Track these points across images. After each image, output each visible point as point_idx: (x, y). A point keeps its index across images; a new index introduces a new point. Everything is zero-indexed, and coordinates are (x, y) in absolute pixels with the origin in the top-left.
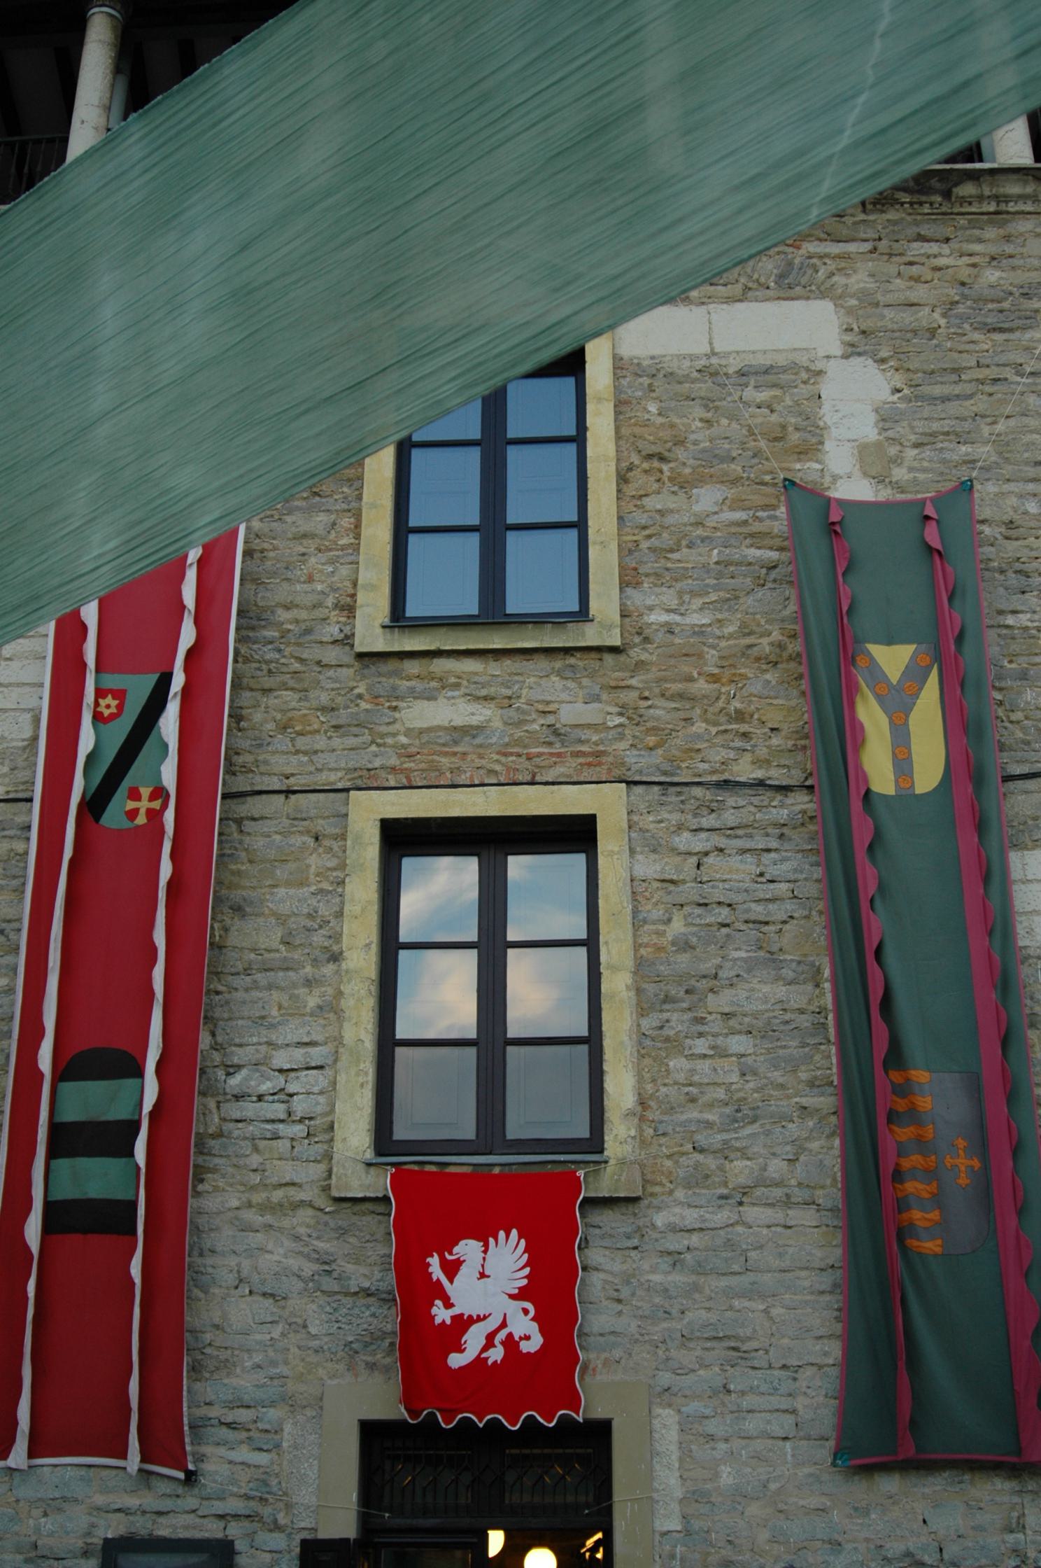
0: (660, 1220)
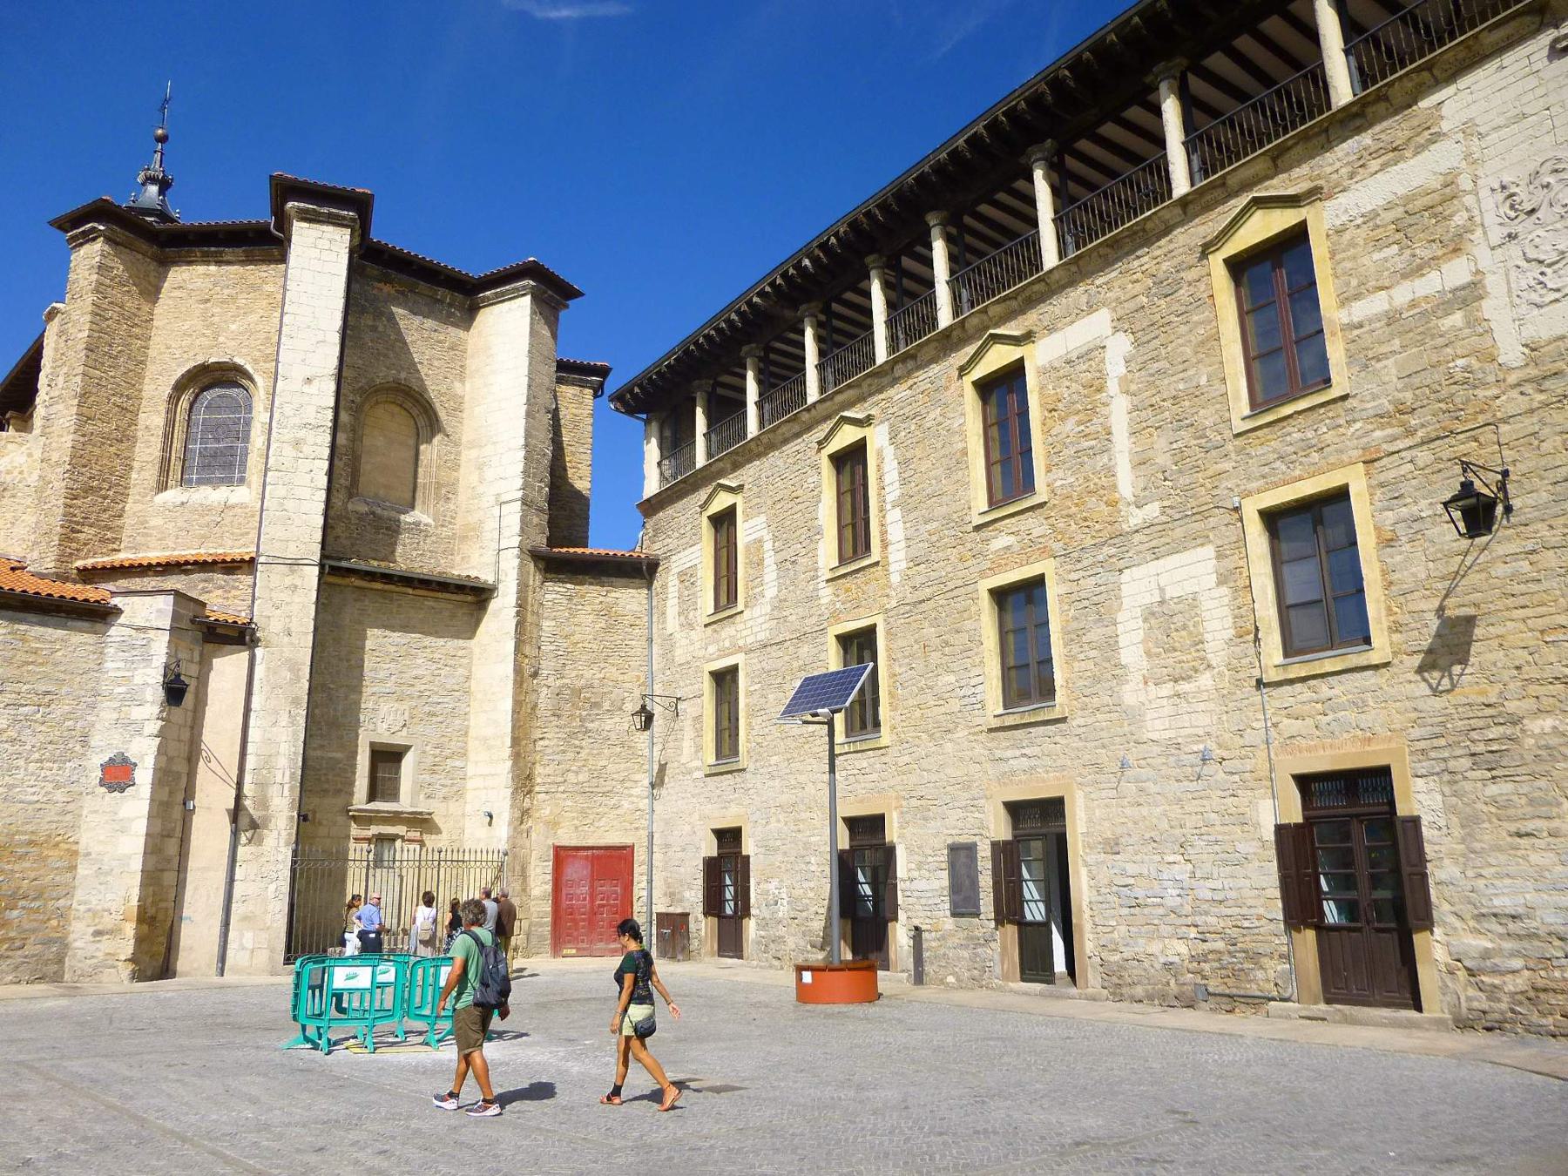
0: (1074, 723)
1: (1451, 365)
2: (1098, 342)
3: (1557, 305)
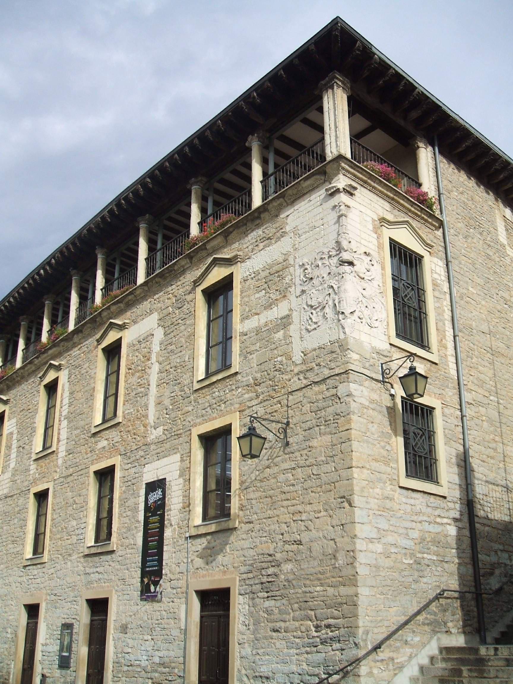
1: (276, 360)
2: (148, 333)
3: (315, 331)
